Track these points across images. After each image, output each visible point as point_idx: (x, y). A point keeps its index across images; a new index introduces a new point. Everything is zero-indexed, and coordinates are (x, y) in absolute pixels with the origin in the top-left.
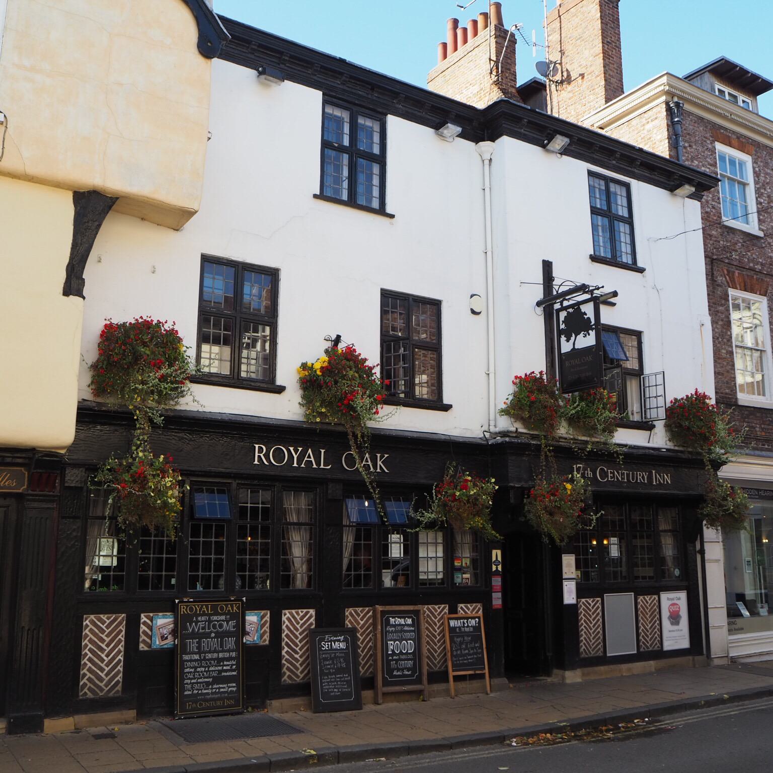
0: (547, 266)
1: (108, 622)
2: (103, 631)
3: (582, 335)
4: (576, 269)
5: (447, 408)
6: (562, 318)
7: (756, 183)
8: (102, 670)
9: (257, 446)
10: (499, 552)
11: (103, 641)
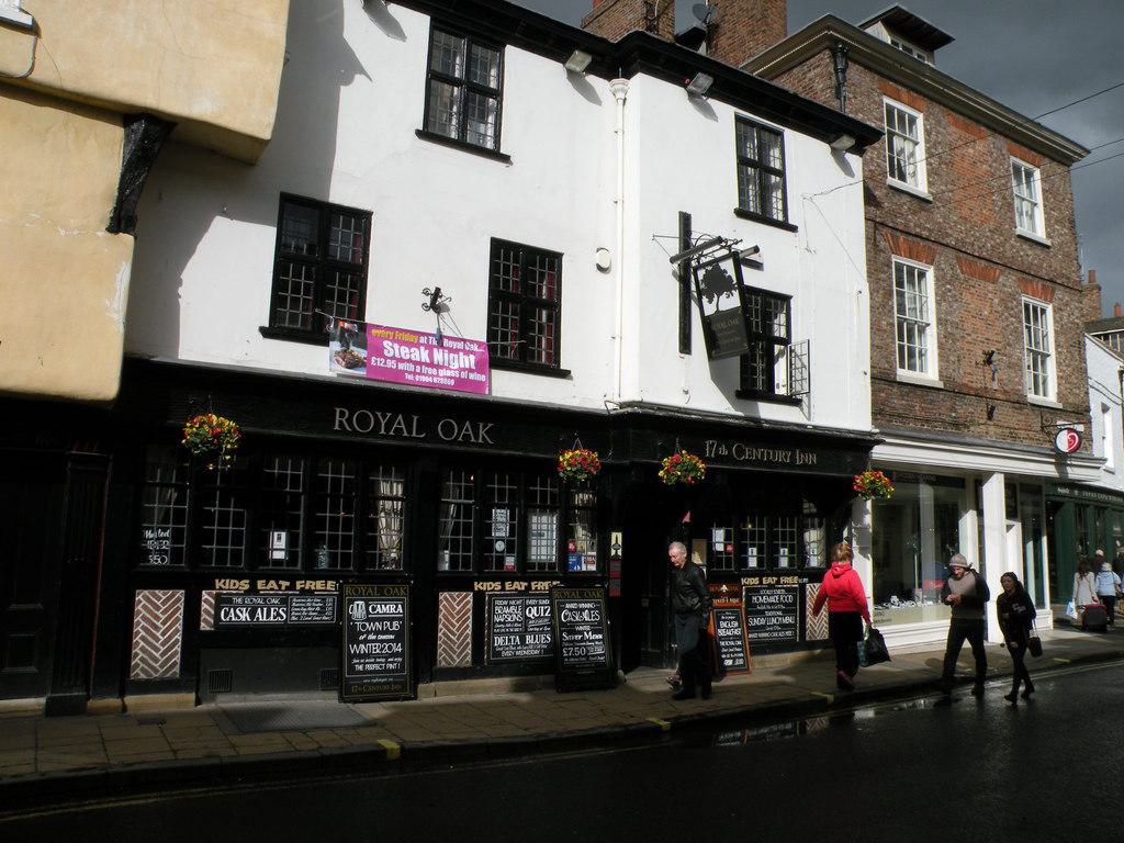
0: (685, 220)
1: (164, 598)
2: (158, 608)
3: (724, 295)
4: (718, 218)
5: (565, 374)
6: (700, 277)
7: (927, 141)
8: (157, 650)
9: (338, 410)
10: (620, 535)
11: (158, 618)
